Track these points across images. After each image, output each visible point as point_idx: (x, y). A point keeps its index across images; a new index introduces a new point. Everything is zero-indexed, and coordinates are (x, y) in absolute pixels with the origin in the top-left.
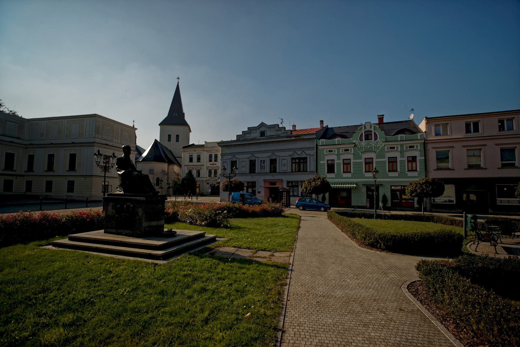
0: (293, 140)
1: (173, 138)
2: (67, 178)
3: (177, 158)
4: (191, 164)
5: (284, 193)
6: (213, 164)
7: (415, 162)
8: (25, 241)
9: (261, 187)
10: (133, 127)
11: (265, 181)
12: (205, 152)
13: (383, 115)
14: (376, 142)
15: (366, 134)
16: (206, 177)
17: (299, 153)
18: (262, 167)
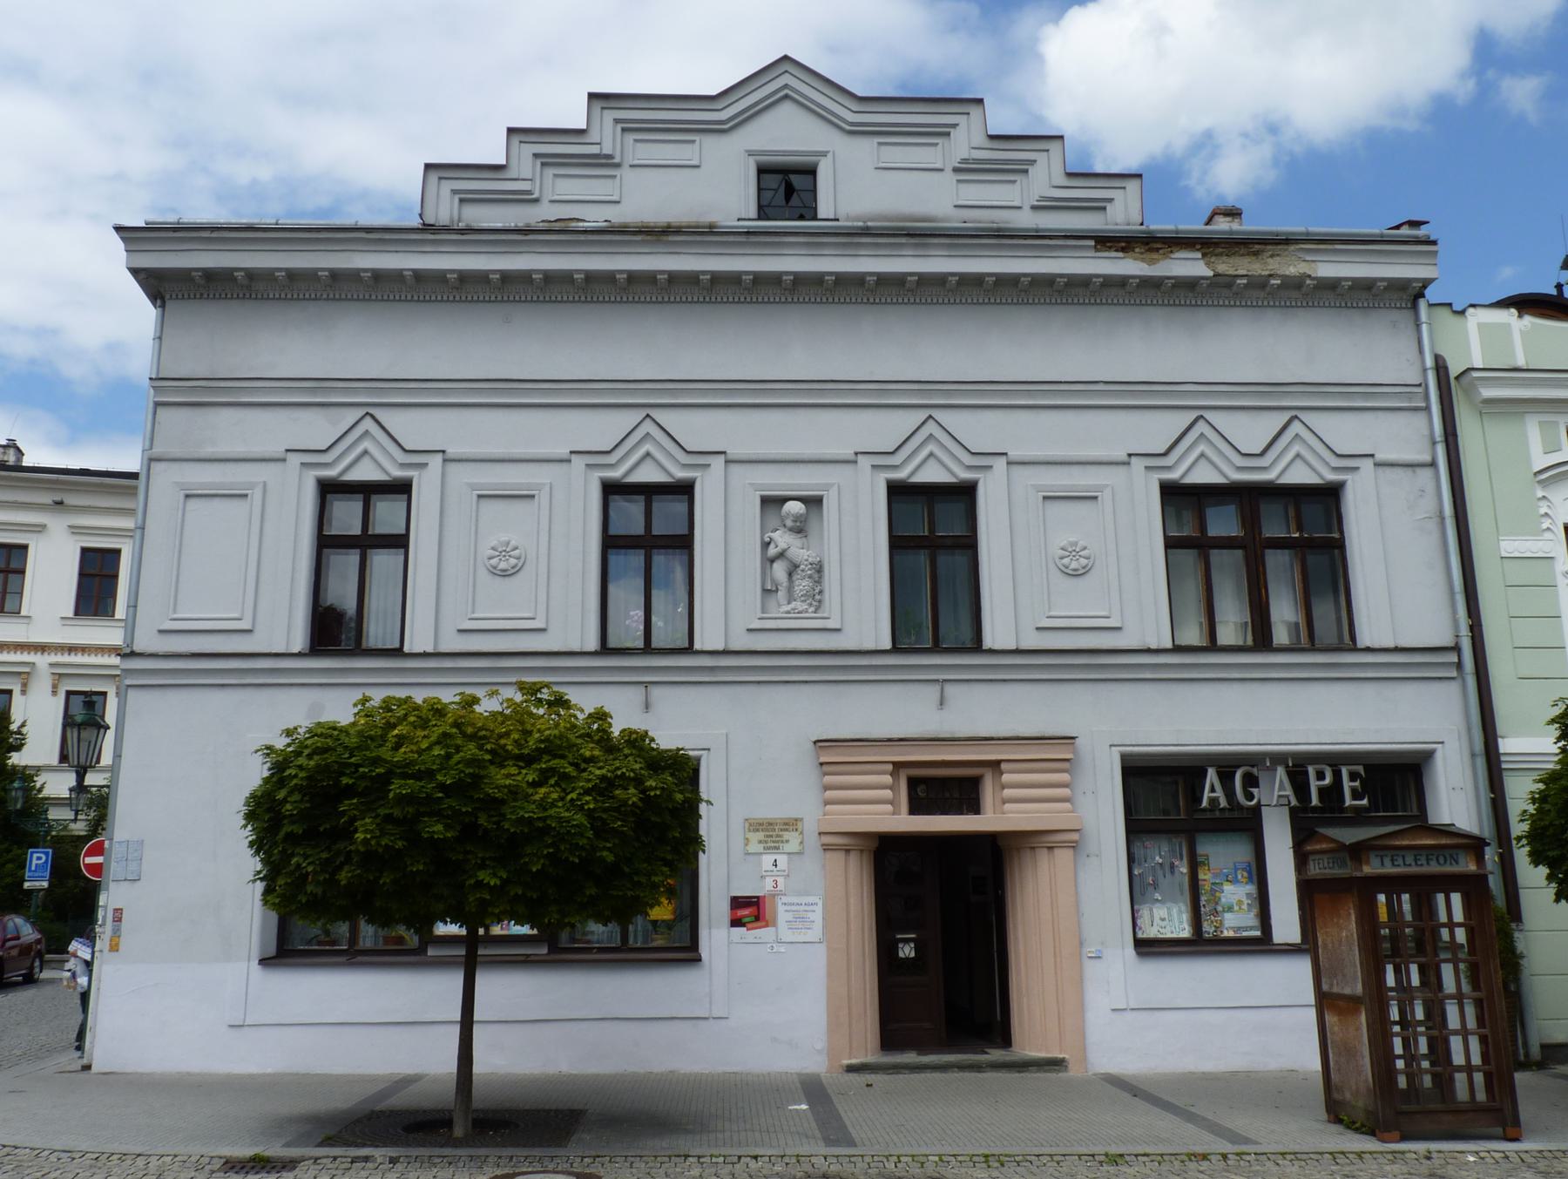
8: (1319, 965)
9: (772, 831)
17: (1251, 431)
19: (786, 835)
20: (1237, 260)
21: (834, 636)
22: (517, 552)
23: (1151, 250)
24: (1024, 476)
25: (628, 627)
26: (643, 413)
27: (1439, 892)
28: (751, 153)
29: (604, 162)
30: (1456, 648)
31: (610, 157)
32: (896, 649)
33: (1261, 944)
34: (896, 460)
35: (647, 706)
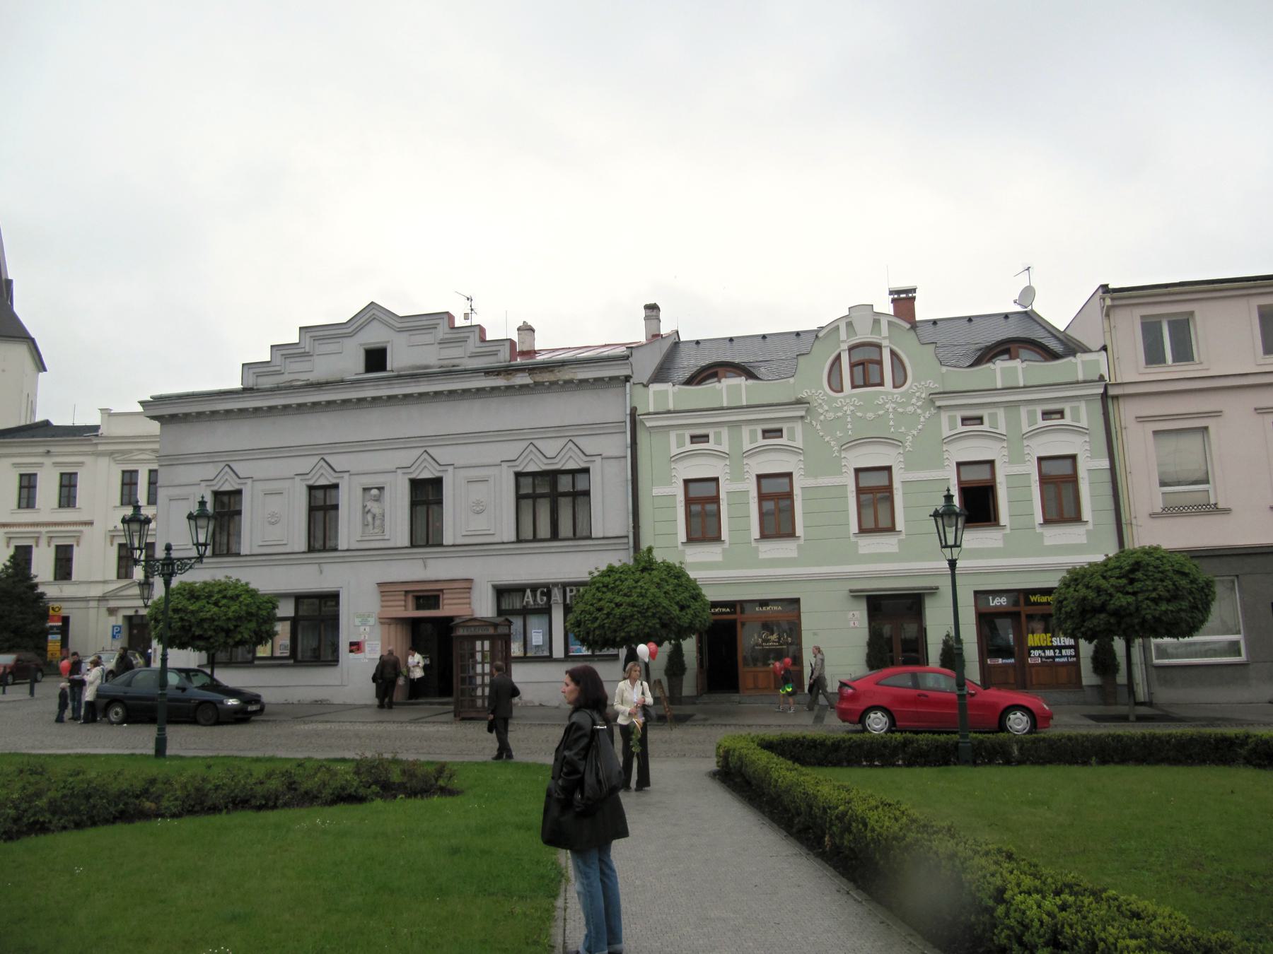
0: (522, 386)
4: (26, 516)
5: (478, 644)
11: (386, 589)
12: (104, 462)
13: (914, 290)
14: (902, 395)
15: (856, 359)
16: (105, 582)
18: (372, 520)
19: (369, 619)
20: (543, 375)
21: (189, 551)
23: (508, 374)
25: (527, 533)
26: (568, 439)
27: (478, 640)
28: (361, 345)
29: (306, 354)
30: (627, 537)
31: (308, 353)
33: (549, 659)
34: (516, 463)
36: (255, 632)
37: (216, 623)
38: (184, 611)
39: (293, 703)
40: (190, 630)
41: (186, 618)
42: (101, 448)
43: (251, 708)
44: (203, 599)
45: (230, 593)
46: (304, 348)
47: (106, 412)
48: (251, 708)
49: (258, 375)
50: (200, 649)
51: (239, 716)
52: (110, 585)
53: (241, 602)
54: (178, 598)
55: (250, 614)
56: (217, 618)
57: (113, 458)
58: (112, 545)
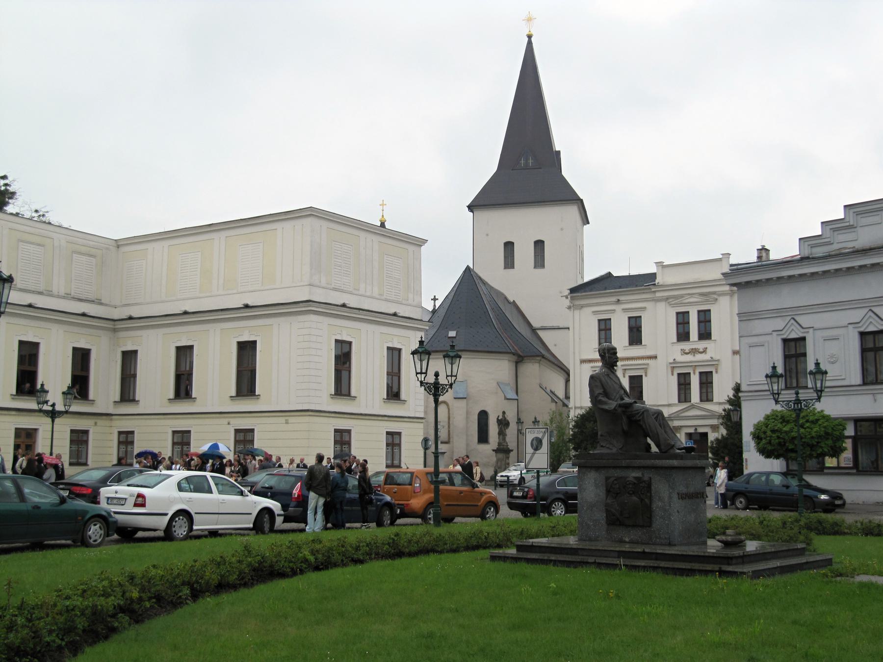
1: (524, 254)
2: (232, 421)
3: (541, 333)
6: (694, 351)
7: (553, 442)
10: (383, 225)
12: (661, 306)
22: (835, 356)
24: (818, 333)
29: (851, 227)
31: (853, 225)
32: (865, 383)
35: (875, 400)
36: (831, 447)
37: (803, 440)
38: (779, 432)
39: (858, 504)
40: (785, 445)
41: (781, 436)
42: (658, 295)
43: (838, 502)
44: (791, 423)
45: (811, 418)
46: (849, 222)
47: (659, 264)
48: (838, 502)
49: (812, 246)
50: (777, 457)
51: (830, 507)
52: (673, 407)
53: (820, 425)
54: (774, 422)
55: (827, 433)
56: (804, 437)
57: (668, 302)
58: (673, 374)
